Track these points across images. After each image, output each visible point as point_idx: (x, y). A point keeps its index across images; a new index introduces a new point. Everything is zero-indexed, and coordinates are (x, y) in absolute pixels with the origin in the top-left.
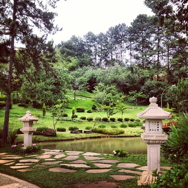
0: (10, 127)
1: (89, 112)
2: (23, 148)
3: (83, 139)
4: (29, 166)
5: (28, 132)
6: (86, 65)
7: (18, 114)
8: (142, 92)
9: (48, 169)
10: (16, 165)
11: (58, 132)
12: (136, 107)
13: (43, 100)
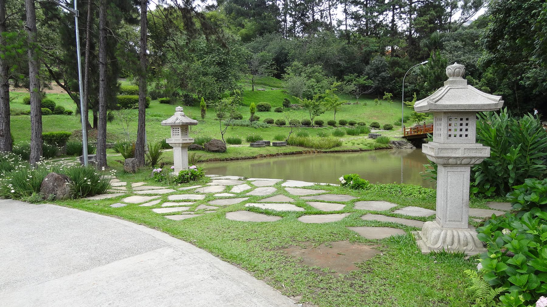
0: (147, 143)
1: (278, 111)
2: (172, 173)
3: (271, 156)
4: (187, 208)
5: (181, 145)
6: (270, 32)
7: (160, 116)
8: (367, 77)
9: (225, 214)
10: (163, 206)
11: (228, 145)
12: (356, 102)
13: (200, 92)
